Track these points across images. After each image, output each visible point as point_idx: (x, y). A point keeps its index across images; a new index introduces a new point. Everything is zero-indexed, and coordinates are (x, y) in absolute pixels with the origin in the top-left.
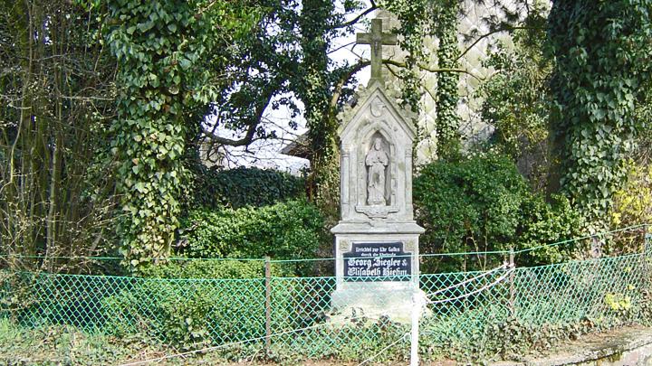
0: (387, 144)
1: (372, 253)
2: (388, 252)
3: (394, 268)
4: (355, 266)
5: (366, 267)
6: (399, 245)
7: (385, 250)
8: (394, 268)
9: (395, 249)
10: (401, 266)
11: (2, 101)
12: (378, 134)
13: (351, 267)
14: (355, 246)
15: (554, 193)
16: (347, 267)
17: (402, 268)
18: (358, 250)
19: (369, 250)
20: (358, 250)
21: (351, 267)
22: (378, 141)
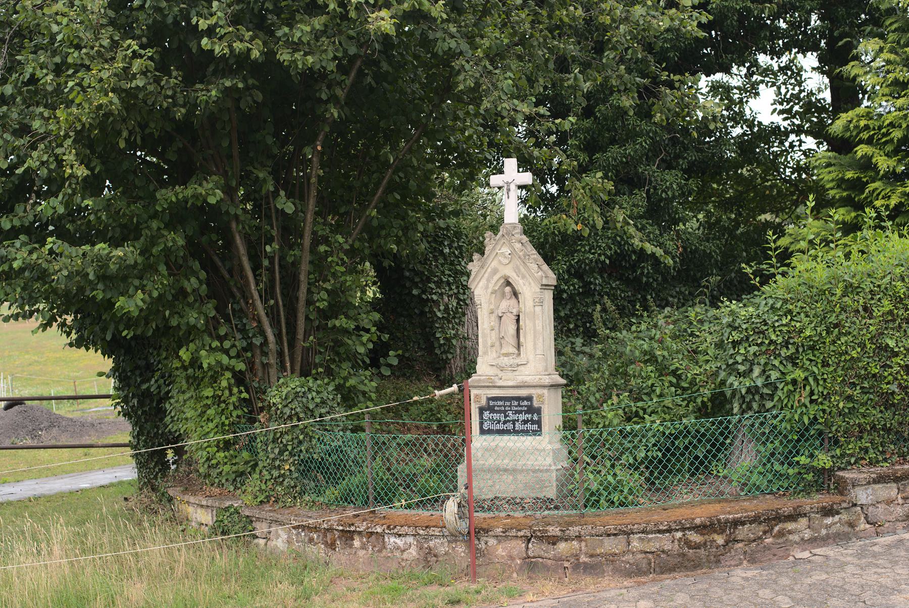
0: (515, 294)
1: (505, 407)
2: (519, 405)
3: (525, 422)
6: (529, 398)
7: (516, 403)
9: (526, 403)
12: (508, 283)
14: (489, 399)
17: (533, 422)
18: (491, 403)
20: (491, 403)
22: (508, 289)
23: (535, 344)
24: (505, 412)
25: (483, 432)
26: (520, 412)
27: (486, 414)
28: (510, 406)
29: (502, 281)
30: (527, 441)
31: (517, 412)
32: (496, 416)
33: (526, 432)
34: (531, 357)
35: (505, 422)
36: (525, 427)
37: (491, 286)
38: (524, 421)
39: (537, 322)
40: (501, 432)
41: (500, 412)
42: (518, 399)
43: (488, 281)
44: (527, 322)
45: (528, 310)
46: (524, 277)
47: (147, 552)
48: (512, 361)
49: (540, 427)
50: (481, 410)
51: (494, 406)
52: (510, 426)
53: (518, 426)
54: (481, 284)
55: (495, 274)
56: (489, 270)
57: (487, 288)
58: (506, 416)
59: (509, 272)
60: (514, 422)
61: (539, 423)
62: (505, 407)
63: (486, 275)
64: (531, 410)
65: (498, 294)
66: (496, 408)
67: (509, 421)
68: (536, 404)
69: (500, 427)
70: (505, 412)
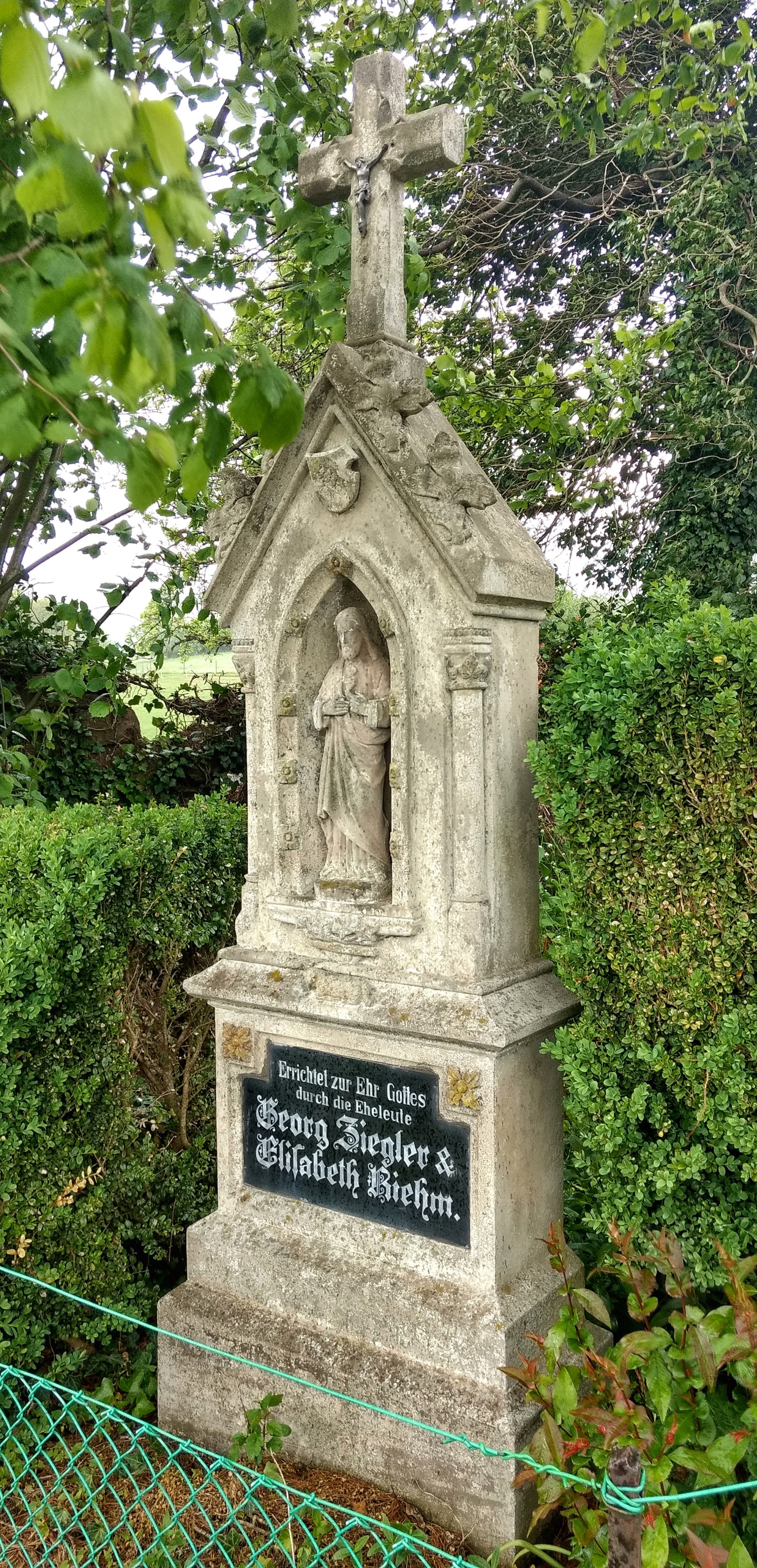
0: (375, 640)
1: (332, 1095)
2: (381, 1101)
3: (405, 1174)
4: (279, 1135)
5: (310, 1146)
6: (422, 1080)
7: (371, 1089)
8: (405, 1174)
9: (406, 1096)
10: (430, 1172)
11: (606, 5)
12: (348, 593)
13: (266, 1133)
14: (278, 1053)
15: (134, 732)
16: (252, 1134)
17: (436, 1184)
18: (285, 1071)
19: (318, 1078)
20: (285, 1071)
21: (266, 1133)
22: (345, 619)
23: (449, 856)
24: (331, 1114)
25: (255, 1175)
26: (386, 1129)
27: (266, 1106)
28: (351, 1096)
29: (327, 583)
30: (420, 1257)
31: (373, 1126)
32: (299, 1124)
33: (406, 1217)
34: (432, 908)
35: (331, 1156)
36: (393, 1192)
37: (286, 602)
38: (397, 1166)
39: (460, 759)
40: (321, 1193)
41: (310, 1110)
42: (380, 1073)
43: (278, 583)
44: (421, 755)
45: (422, 711)
46: (409, 563)
47: (244, 1544)
48: (354, 919)
49: (462, 1205)
50: (252, 1091)
51: (293, 1085)
52: (345, 1174)
53: (377, 1181)
54: (254, 597)
55: (302, 553)
56: (282, 539)
57: (273, 612)
58: (335, 1133)
59: (350, 539)
60: (364, 1162)
61: (458, 1189)
62: (332, 1095)
63: (272, 559)
64: (426, 1128)
65: (316, 638)
66: (300, 1094)
67: (346, 1155)
68: (449, 1112)
69: (308, 1167)
70: (331, 1114)
